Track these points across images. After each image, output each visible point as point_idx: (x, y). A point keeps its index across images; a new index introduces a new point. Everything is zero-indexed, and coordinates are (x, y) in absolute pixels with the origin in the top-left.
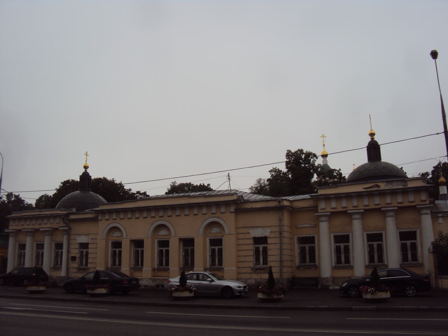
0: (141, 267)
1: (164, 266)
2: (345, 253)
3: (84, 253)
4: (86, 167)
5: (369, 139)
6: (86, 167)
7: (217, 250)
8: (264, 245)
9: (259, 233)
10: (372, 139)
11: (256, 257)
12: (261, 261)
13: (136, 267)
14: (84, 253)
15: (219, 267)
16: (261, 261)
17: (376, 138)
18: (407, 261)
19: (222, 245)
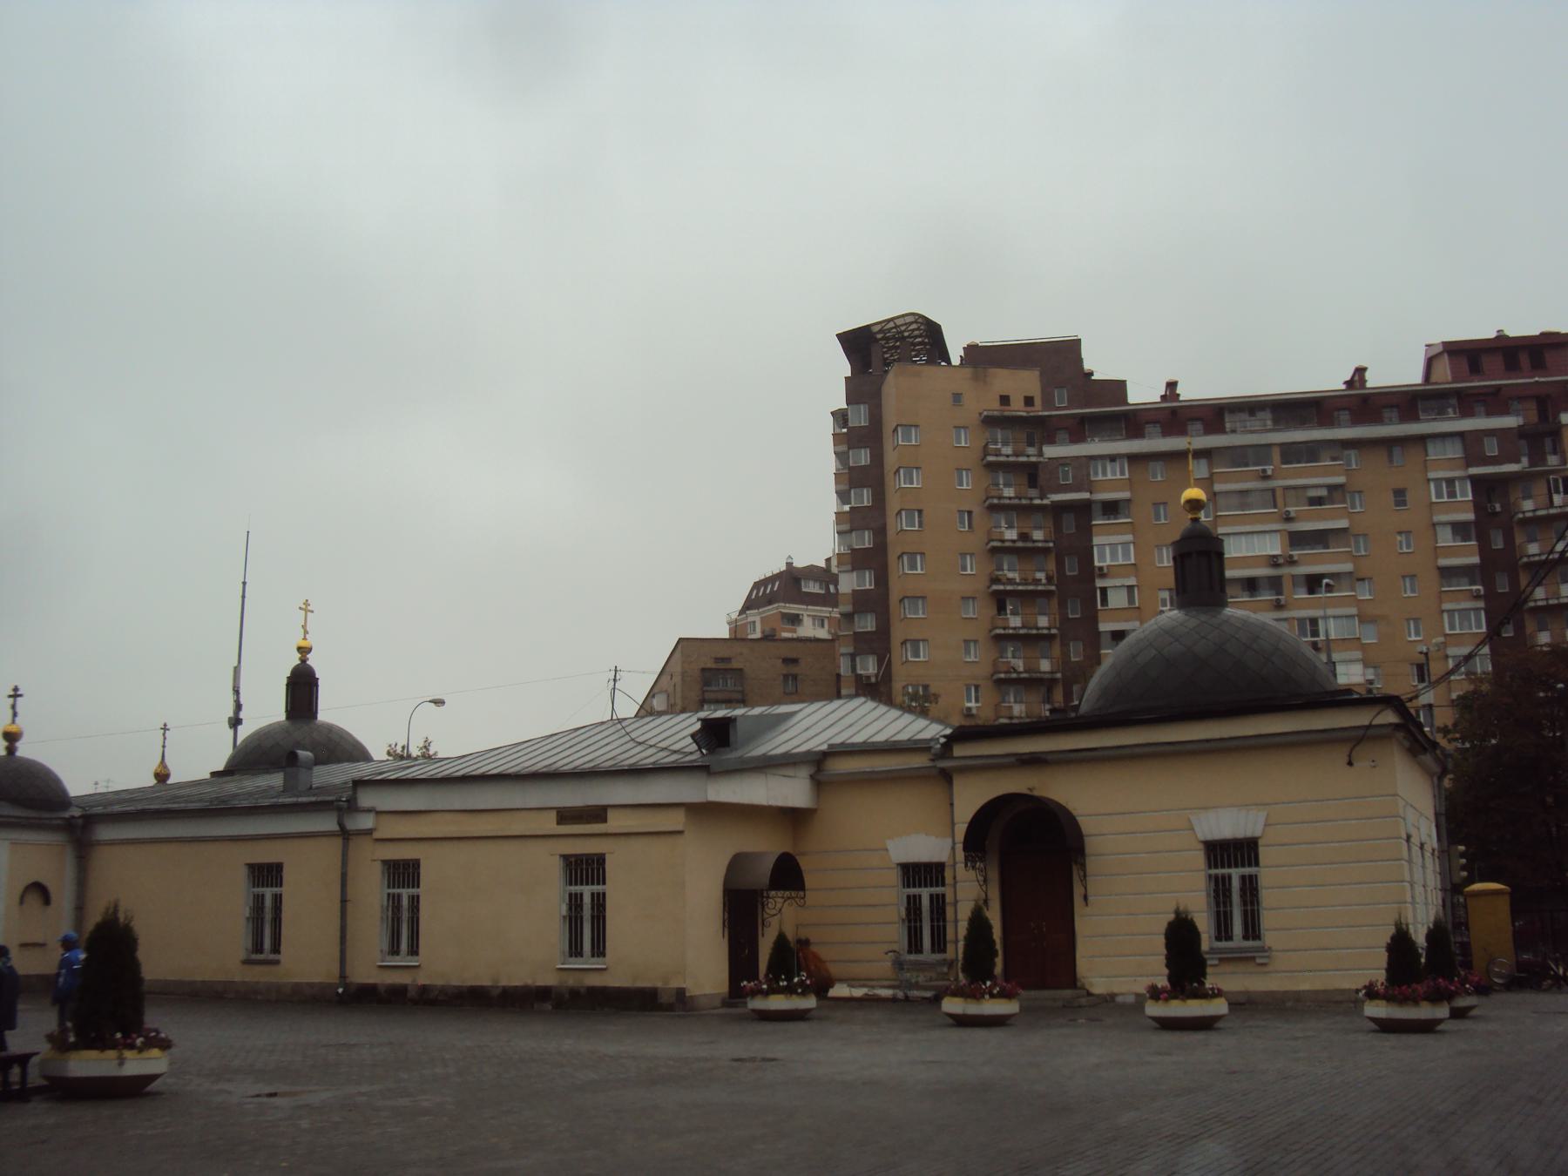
0: (272, 957)
1: (1238, 940)
2: (1244, 903)
3: (405, 902)
4: (304, 651)
5: (295, 660)
6: (304, 651)
7: (587, 899)
8: (1247, 871)
9: (1227, 825)
10: (304, 661)
11: (1218, 913)
12: (404, 946)
13: (254, 957)
14: (405, 902)
15: (1250, 943)
16: (404, 946)
17: (312, 660)
18: (1229, 938)
19: (1257, 864)
